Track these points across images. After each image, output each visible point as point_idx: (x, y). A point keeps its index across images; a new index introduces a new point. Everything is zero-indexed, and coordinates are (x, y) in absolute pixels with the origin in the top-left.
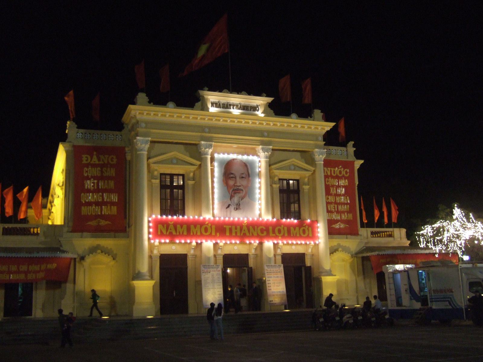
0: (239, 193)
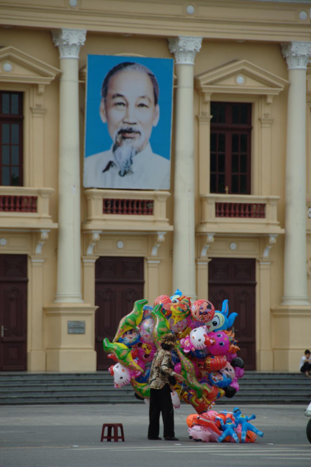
0: (131, 138)
